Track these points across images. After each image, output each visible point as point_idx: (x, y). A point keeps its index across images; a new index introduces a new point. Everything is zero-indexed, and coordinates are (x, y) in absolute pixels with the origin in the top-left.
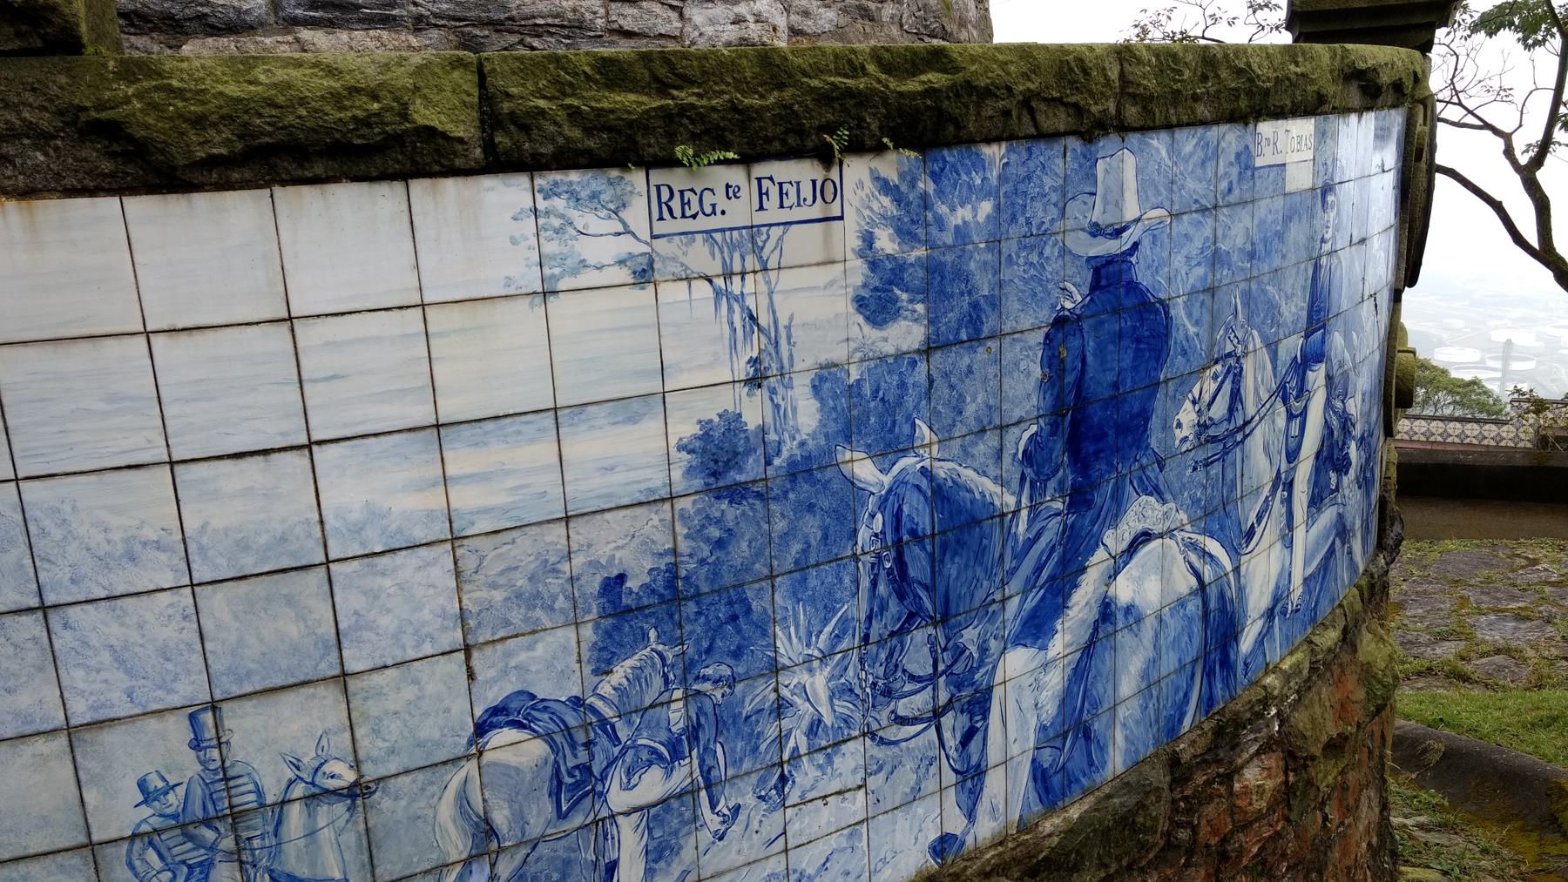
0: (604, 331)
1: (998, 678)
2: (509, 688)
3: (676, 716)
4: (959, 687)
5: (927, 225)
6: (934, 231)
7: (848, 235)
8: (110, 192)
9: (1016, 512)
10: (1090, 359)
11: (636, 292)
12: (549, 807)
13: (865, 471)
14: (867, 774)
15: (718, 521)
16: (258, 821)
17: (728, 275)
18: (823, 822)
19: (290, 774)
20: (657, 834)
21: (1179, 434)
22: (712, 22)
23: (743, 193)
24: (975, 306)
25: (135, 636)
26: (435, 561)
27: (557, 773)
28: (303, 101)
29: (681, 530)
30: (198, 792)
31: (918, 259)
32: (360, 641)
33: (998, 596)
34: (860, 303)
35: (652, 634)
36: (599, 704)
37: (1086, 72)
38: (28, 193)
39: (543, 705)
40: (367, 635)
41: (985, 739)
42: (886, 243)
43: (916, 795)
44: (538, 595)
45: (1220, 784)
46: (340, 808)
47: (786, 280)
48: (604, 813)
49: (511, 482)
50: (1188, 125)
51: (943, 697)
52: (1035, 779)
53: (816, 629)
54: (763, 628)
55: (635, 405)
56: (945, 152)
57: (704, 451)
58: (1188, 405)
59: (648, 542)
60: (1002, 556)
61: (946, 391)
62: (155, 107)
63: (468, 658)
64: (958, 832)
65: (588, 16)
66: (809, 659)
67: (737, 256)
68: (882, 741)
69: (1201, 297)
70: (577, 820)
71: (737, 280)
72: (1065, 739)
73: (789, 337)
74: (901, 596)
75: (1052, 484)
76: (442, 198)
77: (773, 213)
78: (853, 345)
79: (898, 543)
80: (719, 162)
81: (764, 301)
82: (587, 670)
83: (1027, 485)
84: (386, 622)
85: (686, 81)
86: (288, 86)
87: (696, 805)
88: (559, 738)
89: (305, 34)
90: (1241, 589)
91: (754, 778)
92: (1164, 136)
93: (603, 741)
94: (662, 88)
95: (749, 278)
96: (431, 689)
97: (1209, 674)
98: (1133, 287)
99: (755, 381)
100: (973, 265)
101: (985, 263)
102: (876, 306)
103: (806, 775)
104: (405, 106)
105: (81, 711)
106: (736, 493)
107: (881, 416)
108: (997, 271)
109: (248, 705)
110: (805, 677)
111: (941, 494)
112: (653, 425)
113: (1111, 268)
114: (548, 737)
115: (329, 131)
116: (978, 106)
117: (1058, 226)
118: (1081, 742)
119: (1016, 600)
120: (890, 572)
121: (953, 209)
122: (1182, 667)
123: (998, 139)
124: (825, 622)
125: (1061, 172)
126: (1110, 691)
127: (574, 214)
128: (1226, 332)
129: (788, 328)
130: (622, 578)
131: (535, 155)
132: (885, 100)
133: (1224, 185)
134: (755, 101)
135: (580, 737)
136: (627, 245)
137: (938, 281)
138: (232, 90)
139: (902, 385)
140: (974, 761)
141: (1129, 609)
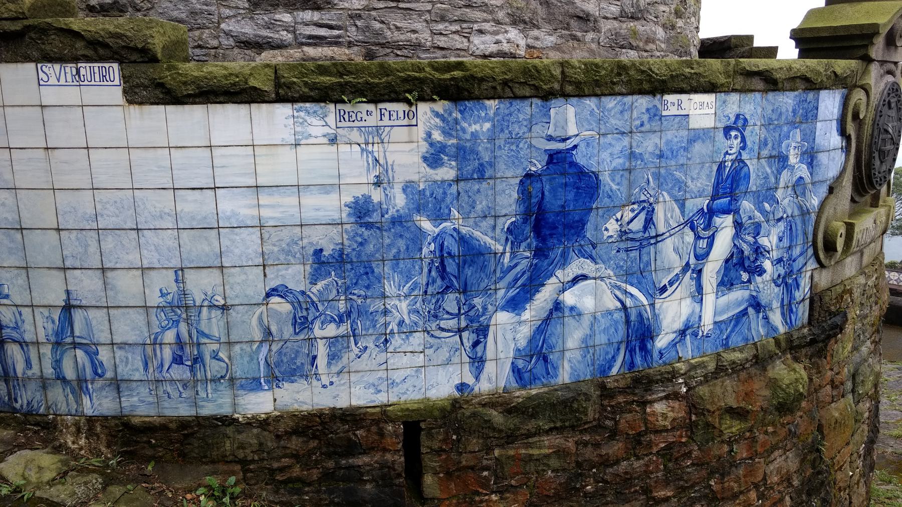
0: (316, 159)
1: (493, 322)
2: (278, 283)
3: (342, 306)
4: (472, 321)
5: (457, 131)
6: (461, 133)
7: (420, 132)
8: (162, 104)
9: (503, 253)
10: (546, 193)
11: (330, 147)
12: (291, 329)
13: (427, 225)
14: (425, 348)
15: (361, 235)
16: (193, 311)
17: (367, 143)
18: (404, 362)
19: (203, 297)
20: (333, 349)
21: (606, 234)
22: (483, 43)
23: (374, 114)
24: (481, 165)
25: (161, 242)
26: (254, 233)
27: (295, 317)
28: (215, 78)
29: (344, 235)
30: (176, 296)
31: (453, 144)
32: (228, 256)
33: (493, 287)
34: (425, 159)
35: (333, 273)
36: (311, 295)
37: (538, 71)
38: (141, 103)
39: (291, 291)
40: (230, 255)
41: (485, 347)
42: (437, 136)
43: (448, 362)
44: (290, 251)
45: (637, 406)
46: (219, 312)
47: (391, 147)
48: (312, 336)
49: (281, 209)
50: (610, 95)
51: (463, 324)
52: (513, 371)
53: (403, 284)
54: (379, 279)
55: (328, 188)
56: (466, 102)
57: (355, 208)
58: (613, 221)
59: (332, 239)
60: (495, 271)
61: (466, 198)
62: (174, 79)
63: (264, 269)
64: (471, 384)
65: (423, 41)
66: (399, 296)
67: (371, 137)
68: (432, 336)
69: (621, 173)
70: (302, 336)
71: (370, 146)
72: (532, 358)
73: (392, 169)
74: (443, 278)
75: (523, 245)
76: (261, 111)
77: (386, 121)
78: (421, 175)
79: (442, 257)
80: (359, 102)
81: (382, 154)
82: (308, 282)
83: (509, 243)
84: (237, 251)
85: (350, 73)
86: (211, 72)
87: (349, 342)
88: (296, 305)
89: (306, 49)
90: (656, 316)
91: (374, 337)
92: (594, 99)
93: (313, 309)
94: (341, 75)
95: (376, 145)
96: (250, 277)
97: (631, 351)
98: (573, 164)
99: (378, 184)
100: (480, 148)
101: (487, 148)
102: (433, 159)
103: (397, 341)
104: (246, 80)
105: (146, 265)
106: (369, 226)
107: (434, 204)
108: (493, 151)
109: (192, 271)
110: (397, 302)
111: (463, 240)
112: (334, 196)
113: (559, 155)
114: (292, 303)
115: (223, 87)
116: (479, 85)
117: (527, 135)
118: (541, 362)
119: (503, 291)
120: (437, 268)
121: (470, 125)
122: (610, 343)
123: (493, 98)
124: (407, 282)
125: (529, 112)
126: (560, 342)
127: (307, 118)
128: (641, 190)
129: (392, 165)
130: (321, 250)
131: (293, 97)
132: (432, 81)
133: (638, 123)
134: (377, 81)
135: (304, 306)
136: (327, 130)
137: (462, 154)
138: (196, 74)
139: (445, 193)
140: (479, 355)
141: (572, 309)
